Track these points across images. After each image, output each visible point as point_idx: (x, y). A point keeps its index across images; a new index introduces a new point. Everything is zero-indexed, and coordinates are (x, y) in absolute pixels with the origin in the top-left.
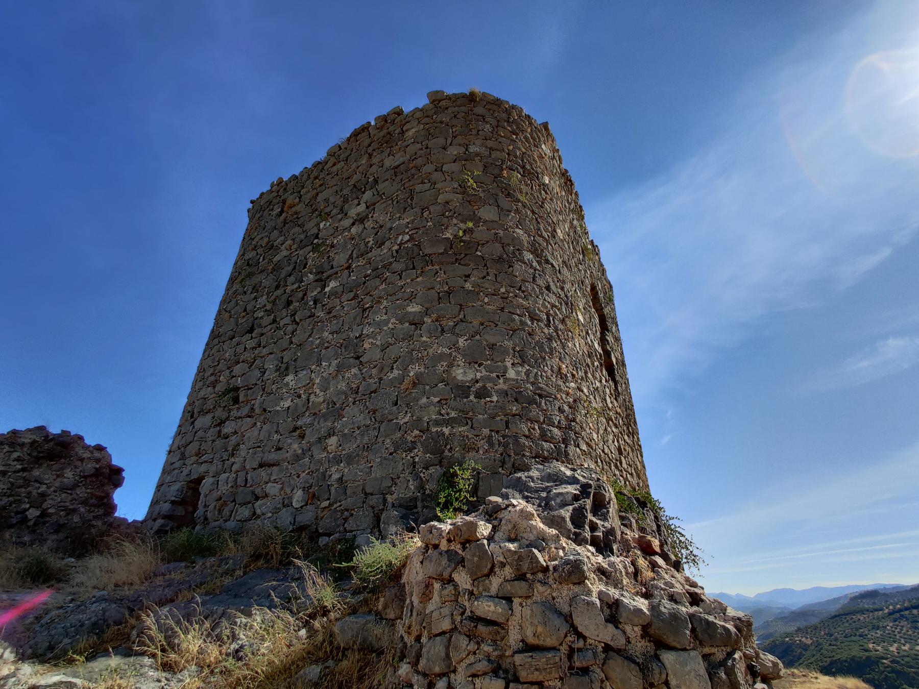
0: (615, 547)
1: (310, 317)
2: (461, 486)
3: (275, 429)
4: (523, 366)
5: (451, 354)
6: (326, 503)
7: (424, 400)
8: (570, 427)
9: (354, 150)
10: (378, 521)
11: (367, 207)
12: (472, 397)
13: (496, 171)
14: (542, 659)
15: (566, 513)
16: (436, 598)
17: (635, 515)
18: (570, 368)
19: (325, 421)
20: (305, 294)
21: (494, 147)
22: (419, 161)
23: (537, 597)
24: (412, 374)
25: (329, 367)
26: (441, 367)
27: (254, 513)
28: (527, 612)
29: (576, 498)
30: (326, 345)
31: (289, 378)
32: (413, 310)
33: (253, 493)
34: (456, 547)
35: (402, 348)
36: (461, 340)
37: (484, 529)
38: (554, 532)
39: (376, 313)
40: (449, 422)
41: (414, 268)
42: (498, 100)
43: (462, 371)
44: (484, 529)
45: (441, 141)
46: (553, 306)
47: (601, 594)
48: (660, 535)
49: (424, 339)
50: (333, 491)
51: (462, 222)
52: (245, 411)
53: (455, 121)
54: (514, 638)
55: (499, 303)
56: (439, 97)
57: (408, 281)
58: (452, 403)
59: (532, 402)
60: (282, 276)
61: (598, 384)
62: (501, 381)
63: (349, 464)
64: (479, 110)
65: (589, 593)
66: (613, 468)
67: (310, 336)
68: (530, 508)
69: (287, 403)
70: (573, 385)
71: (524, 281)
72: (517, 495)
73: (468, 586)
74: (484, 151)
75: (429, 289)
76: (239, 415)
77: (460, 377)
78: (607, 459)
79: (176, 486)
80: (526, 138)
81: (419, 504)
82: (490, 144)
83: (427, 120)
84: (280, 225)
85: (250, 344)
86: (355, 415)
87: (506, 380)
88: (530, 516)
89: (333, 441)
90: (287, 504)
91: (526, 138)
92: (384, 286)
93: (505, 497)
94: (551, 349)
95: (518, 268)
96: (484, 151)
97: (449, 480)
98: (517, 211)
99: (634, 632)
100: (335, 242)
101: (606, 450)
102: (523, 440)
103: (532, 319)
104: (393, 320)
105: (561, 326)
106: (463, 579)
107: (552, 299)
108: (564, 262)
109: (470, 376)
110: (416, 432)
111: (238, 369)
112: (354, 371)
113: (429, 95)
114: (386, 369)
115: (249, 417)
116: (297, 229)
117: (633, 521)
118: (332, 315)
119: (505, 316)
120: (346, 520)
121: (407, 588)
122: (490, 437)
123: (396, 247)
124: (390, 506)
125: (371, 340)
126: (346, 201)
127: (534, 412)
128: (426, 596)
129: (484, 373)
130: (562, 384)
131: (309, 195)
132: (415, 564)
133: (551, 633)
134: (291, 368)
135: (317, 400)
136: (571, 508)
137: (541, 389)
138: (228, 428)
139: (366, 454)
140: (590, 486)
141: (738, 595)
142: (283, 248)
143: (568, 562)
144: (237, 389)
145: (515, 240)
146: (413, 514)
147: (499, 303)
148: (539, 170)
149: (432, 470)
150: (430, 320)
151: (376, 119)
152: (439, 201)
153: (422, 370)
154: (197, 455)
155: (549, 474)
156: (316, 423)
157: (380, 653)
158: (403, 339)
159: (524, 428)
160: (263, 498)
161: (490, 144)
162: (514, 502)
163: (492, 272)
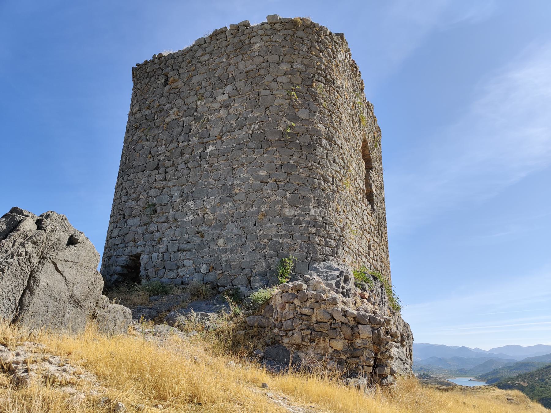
0: (350, 295)
1: (198, 167)
2: (288, 267)
3: (185, 231)
4: (318, 208)
5: (282, 201)
6: (221, 272)
7: (269, 224)
8: (340, 239)
9: (216, 48)
10: (250, 282)
11: (229, 97)
12: (293, 224)
13: (309, 83)
14: (322, 325)
15: (334, 282)
16: (287, 309)
17: (369, 284)
18: (343, 206)
19: (216, 230)
20: (193, 151)
21: (309, 64)
22: (262, 72)
23: (322, 308)
24: (263, 210)
25: (214, 200)
26: (278, 207)
27: (178, 275)
28: (318, 312)
29: (338, 277)
30: (211, 186)
31: (190, 203)
32: (262, 174)
33: (176, 264)
34: (295, 292)
35: (257, 195)
36: (288, 194)
37: (305, 286)
38: (328, 288)
39: (240, 172)
40: (281, 236)
41: (261, 148)
42: (312, 23)
43: (288, 210)
44: (305, 286)
45: (275, 58)
46: (336, 171)
47: (342, 309)
48: (382, 294)
49: (269, 191)
50: (223, 266)
51: (289, 120)
52: (163, 219)
53: (284, 43)
54: (314, 320)
55: (307, 172)
56: (274, 21)
57: (259, 155)
58: (283, 227)
59: (322, 227)
60: (175, 133)
61: (359, 210)
62: (307, 216)
63: (231, 253)
64: (300, 34)
65: (338, 307)
66: (363, 258)
67: (200, 179)
68: (321, 280)
69: (191, 218)
70: (344, 216)
71: (321, 158)
72: (315, 274)
73: (299, 305)
74: (302, 68)
75: (271, 162)
76: (159, 220)
77: (287, 214)
78: (360, 254)
79: (124, 258)
80: (328, 53)
81: (268, 274)
82: (306, 61)
83: (265, 38)
84: (166, 94)
85: (159, 177)
86: (232, 229)
87: (310, 216)
88: (320, 283)
89: (221, 241)
90: (197, 270)
91: (328, 53)
92: (244, 156)
93: (311, 275)
94: (333, 197)
95: (319, 150)
96: (302, 68)
97: (283, 264)
98: (320, 112)
99: (351, 319)
100: (210, 118)
101: (360, 249)
102: (317, 246)
103: (324, 181)
104: (251, 179)
105: (340, 184)
106: (297, 302)
107: (336, 167)
108: (345, 140)
109: (292, 213)
110: (266, 240)
111: (152, 192)
112: (230, 204)
113: (268, 17)
114: (249, 206)
115: (166, 222)
116: (180, 101)
117: (367, 287)
118: (213, 168)
119: (310, 180)
120: (232, 280)
121: (274, 307)
122: (301, 244)
123: (250, 132)
124: (254, 275)
125: (239, 188)
126: (214, 89)
127: (323, 232)
128: (283, 307)
129: (299, 212)
130: (338, 216)
131: (186, 75)
132: (278, 297)
133: (326, 318)
134: (190, 197)
135: (209, 218)
136: (335, 280)
137: (326, 220)
138: (153, 228)
139: (240, 249)
140: (344, 272)
141: (476, 349)
142: (171, 112)
143: (332, 298)
144: (154, 205)
145: (318, 132)
146: (265, 279)
147: (307, 172)
148: (335, 77)
149: (274, 259)
150: (271, 181)
151: (231, 26)
152: (275, 104)
153: (268, 208)
154: (133, 241)
155: (328, 266)
156: (210, 231)
157: (265, 327)
158: (258, 191)
159: (317, 240)
160: (182, 267)
161: (306, 61)
162: (315, 277)
163: (305, 153)
